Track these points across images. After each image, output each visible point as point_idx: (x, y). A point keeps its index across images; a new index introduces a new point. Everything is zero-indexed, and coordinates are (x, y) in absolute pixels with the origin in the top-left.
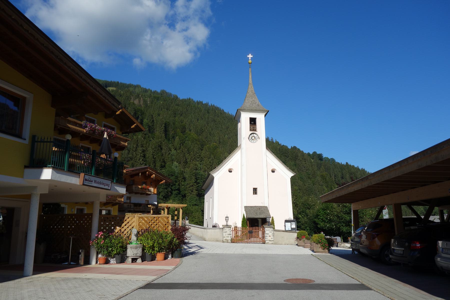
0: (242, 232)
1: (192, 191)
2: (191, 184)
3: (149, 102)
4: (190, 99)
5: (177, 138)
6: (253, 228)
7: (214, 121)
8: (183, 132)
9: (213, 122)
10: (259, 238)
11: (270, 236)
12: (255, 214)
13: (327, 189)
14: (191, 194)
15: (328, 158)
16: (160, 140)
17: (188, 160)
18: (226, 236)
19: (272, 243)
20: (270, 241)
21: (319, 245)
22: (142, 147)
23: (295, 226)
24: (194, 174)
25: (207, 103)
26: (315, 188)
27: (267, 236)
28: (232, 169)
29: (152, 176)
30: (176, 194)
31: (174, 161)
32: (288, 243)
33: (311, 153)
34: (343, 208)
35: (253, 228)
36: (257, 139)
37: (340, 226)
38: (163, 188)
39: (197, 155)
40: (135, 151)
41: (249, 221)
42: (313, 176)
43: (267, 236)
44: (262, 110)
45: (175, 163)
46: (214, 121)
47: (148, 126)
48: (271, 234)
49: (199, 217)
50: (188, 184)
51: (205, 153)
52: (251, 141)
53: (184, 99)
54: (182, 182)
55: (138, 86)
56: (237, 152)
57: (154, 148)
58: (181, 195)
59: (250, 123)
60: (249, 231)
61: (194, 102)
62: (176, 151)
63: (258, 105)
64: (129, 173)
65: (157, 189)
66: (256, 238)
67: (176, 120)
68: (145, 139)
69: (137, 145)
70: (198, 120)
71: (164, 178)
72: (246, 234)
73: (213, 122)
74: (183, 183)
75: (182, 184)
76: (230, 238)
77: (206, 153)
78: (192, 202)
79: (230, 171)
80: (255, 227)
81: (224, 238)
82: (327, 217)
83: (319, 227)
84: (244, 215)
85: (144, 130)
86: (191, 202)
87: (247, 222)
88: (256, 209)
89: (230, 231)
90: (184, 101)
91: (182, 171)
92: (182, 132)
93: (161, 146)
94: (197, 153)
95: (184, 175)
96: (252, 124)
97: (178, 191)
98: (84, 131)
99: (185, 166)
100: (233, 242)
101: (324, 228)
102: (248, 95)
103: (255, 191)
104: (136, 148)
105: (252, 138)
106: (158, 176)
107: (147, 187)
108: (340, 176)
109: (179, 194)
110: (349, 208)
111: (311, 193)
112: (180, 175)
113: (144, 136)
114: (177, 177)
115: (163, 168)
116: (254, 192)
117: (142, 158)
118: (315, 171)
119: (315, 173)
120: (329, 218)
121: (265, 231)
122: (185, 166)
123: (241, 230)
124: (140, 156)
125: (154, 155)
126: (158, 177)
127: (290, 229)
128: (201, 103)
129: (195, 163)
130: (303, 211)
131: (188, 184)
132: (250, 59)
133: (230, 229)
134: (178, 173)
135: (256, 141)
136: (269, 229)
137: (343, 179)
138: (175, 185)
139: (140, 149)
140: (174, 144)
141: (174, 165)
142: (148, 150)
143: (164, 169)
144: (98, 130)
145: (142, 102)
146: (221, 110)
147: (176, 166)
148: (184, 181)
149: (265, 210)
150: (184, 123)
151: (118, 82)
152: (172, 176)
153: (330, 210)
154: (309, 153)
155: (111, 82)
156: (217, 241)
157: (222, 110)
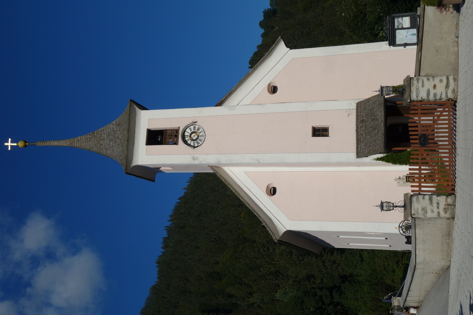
0: (422, 163)
1: (334, 262)
6: (411, 133)
7: (199, 216)
10: (436, 126)
11: (435, 87)
12: (376, 131)
14: (340, 264)
17: (273, 269)
18: (436, 210)
19: (455, 80)
20: (447, 86)
23: (404, 18)
24: (301, 258)
25: (166, 228)
27: (435, 95)
30: (341, 295)
33: (262, 31)
35: (411, 133)
36: (197, 127)
39: (263, 252)
43: (435, 95)
44: (129, 116)
45: (278, 295)
48: (429, 85)
49: (386, 259)
51: (258, 235)
53: (158, 273)
58: (342, 284)
59: (161, 143)
60: (420, 143)
61: (164, 253)
62: (254, 293)
63: (118, 125)
74: (318, 281)
75: (320, 282)
76: (442, 200)
77: (260, 233)
80: (410, 129)
81: (442, 214)
84: (378, 159)
86: (355, 266)
88: (363, 128)
91: (293, 281)
96: (162, 140)
97: (335, 290)
99: (285, 275)
100: (454, 190)
102: (95, 149)
105: (192, 140)
116: (323, 136)
121: (419, 99)
123: (418, 167)
127: (415, 31)
132: (15, 144)
134: (297, 290)
135: (201, 130)
136: (413, 89)
138: (321, 297)
141: (281, 299)
146: (181, 202)
147: (285, 293)
157: (179, 201)
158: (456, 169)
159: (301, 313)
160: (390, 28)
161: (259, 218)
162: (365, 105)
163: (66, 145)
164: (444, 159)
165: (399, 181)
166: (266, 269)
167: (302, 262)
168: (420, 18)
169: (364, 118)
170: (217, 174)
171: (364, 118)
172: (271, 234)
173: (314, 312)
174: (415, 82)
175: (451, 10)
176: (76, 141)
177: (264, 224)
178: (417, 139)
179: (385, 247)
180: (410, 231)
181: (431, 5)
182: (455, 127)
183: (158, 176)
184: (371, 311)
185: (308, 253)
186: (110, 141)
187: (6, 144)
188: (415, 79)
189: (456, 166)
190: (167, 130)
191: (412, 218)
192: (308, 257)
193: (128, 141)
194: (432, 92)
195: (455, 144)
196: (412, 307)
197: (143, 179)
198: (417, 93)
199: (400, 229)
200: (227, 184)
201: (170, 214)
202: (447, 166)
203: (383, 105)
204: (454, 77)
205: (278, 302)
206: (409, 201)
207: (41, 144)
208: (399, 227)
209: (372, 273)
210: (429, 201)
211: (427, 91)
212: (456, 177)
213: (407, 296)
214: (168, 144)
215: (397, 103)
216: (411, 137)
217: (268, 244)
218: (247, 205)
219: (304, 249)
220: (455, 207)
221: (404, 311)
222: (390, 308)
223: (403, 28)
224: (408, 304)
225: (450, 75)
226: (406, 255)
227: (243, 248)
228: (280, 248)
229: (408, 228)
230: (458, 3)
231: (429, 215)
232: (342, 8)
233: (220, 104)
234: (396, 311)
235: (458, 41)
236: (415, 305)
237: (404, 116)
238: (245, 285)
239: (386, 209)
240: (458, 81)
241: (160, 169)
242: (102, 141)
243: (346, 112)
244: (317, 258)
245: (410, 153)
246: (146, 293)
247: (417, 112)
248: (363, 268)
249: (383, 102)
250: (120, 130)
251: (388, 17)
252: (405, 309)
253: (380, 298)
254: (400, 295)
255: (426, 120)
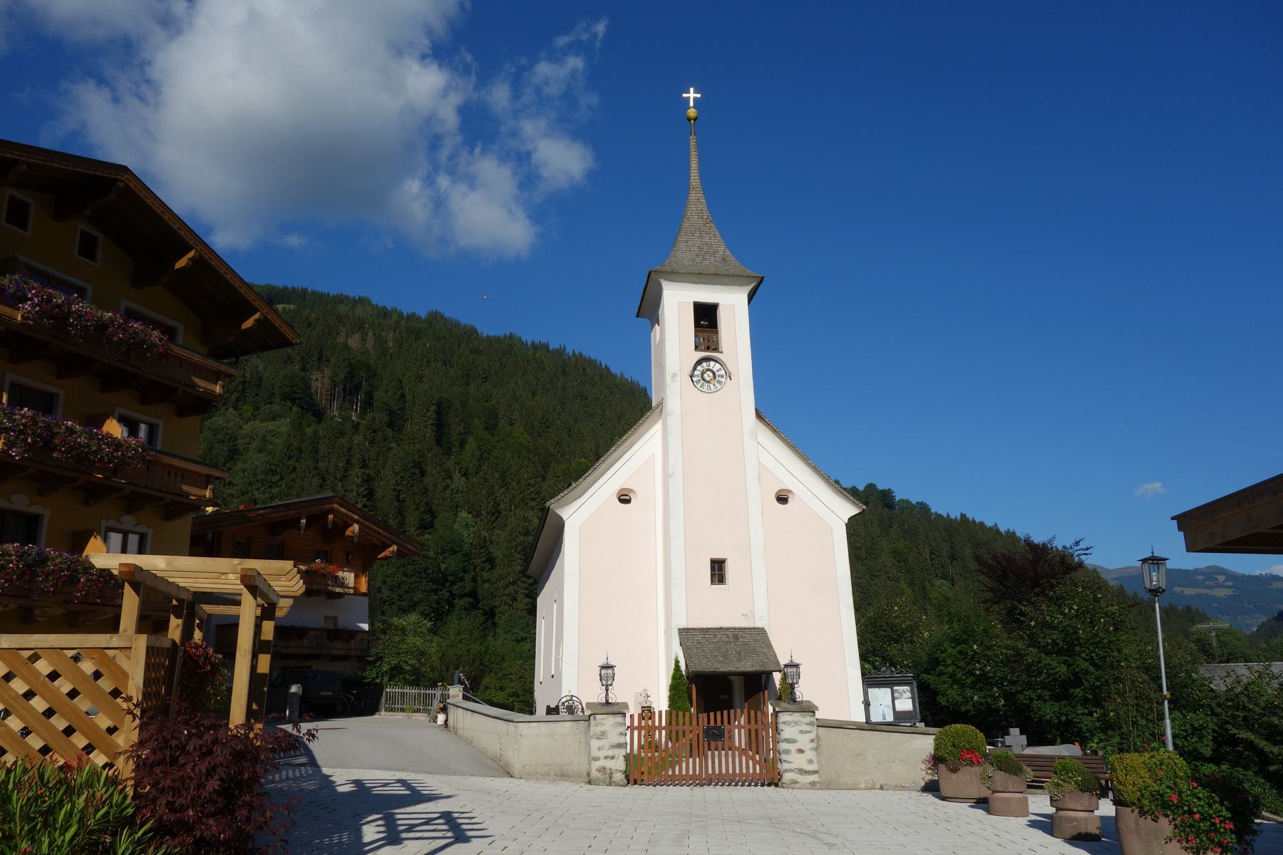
1: (514, 599)
2: (511, 576)
3: (391, 344)
4: (511, 336)
5: (471, 443)
7: (582, 396)
8: (491, 427)
9: (578, 401)
11: (801, 751)
13: (911, 591)
15: (911, 503)
16: (418, 446)
17: (502, 506)
18: (601, 754)
19: (813, 784)
20: (802, 772)
21: (1164, 822)
22: (365, 466)
23: (910, 700)
24: (519, 548)
25: (562, 347)
26: (876, 589)
27: (787, 752)
28: (631, 491)
29: (351, 529)
30: (465, 609)
31: (459, 509)
32: (882, 782)
33: (861, 488)
34: (1043, 632)
36: (723, 380)
37: (1031, 700)
38: (425, 590)
40: (341, 480)
41: (696, 686)
42: (868, 552)
43: (787, 752)
44: (738, 276)
45: (464, 514)
46: (582, 396)
47: (389, 410)
48: (804, 741)
49: (521, 677)
50: (501, 578)
52: (699, 386)
54: (483, 571)
55: (363, 301)
56: (648, 430)
57: (399, 472)
58: (481, 611)
59: (697, 325)
60: (709, 729)
62: (468, 479)
64: (260, 517)
65: (369, 576)
66: (723, 752)
67: (469, 393)
68: (374, 444)
69: (348, 462)
70: (534, 394)
71: (394, 538)
72: (695, 745)
73: (578, 401)
74: (486, 575)
76: (620, 764)
78: (515, 631)
79: (624, 499)
80: (725, 712)
81: (596, 765)
82: (970, 667)
83: (944, 704)
84: (677, 662)
85: (294, 342)
86: (509, 631)
87: (689, 690)
88: (725, 639)
89: (622, 729)
90: (492, 341)
91: (485, 537)
92: (487, 429)
93: (423, 465)
94: (529, 484)
95: (491, 550)
96: (702, 326)
97: (472, 600)
98: (12, 319)
99: (494, 525)
100: (635, 783)
101: (963, 709)
102: (686, 224)
103: (718, 570)
104: (346, 470)
105: (703, 373)
106: (370, 528)
107: (331, 568)
108: (945, 553)
109: (475, 607)
110: (1063, 631)
111: (864, 603)
112: (476, 552)
113: (372, 435)
114: (468, 557)
115: (427, 531)
116: (713, 576)
117: (361, 502)
118: (873, 539)
119: (874, 544)
120: (978, 673)
121: (781, 727)
122: (492, 525)
123: (664, 724)
124: (358, 492)
125: (399, 491)
126: (371, 532)
127: (890, 718)
128: (545, 347)
129: (522, 513)
130: (874, 650)
131: (501, 578)
132: (692, 104)
133: (619, 719)
134: (471, 543)
135: (719, 386)
136: (796, 717)
137: (955, 561)
138: (462, 580)
139: (356, 474)
140: (460, 457)
142: (381, 478)
143: (430, 534)
144: (80, 316)
145: (372, 343)
148: (489, 570)
149: (758, 640)
150: (493, 402)
151: (305, 290)
152: (454, 552)
153: (982, 644)
154: (855, 487)
155: (286, 288)
156: (563, 776)
157: (603, 367)
158: (669, 786)
159: (437, 549)
160: (895, 679)
161: (583, 477)
162: (761, 640)
163: (692, 181)
164: (677, 769)
165: (643, 695)
166: (503, 496)
167: (513, 550)
168: (912, 726)
169: (741, 640)
170: (651, 411)
171: (741, 640)
172: (559, 497)
173: (440, 570)
174: (808, 719)
175: (929, 778)
176: (698, 195)
177: (574, 485)
178: (715, 723)
179: (540, 674)
180: (565, 712)
181: (936, 744)
182: (736, 785)
183: (646, 321)
184: (441, 654)
185: (528, 560)
186: (699, 247)
187: (692, 90)
188: (813, 719)
189: (674, 786)
190: (717, 328)
191: (590, 716)
192: (521, 559)
193: (700, 273)
194: (793, 747)
195: (709, 785)
196: (447, 716)
197: (640, 299)
198: (790, 722)
199: (568, 698)
200: (635, 427)
201: (584, 353)
202: (667, 772)
203: (762, 669)
204: (818, 782)
205: (454, 515)
206: (616, 711)
207: (693, 143)
208: (572, 696)
209: (498, 656)
210: (617, 742)
211: (794, 739)
212: (655, 786)
213: (464, 709)
214: (696, 336)
215: (766, 691)
216: (712, 714)
217: (540, 500)
218: (602, 459)
219: (535, 549)
220: (607, 785)
221: (442, 705)
222: (445, 683)
223: (893, 699)
224: (451, 710)
225: (820, 776)
226: (527, 706)
227: (533, 463)
228: (534, 517)
229: (571, 710)
230: (941, 790)
231: (595, 744)
232: (906, 606)
233: (759, 415)
234: (440, 692)
235: (875, 789)
236: (450, 722)
237: (746, 702)
238: (479, 465)
239: (603, 674)
240: (811, 789)
241: (657, 325)
242: (698, 235)
243: (750, 612)
244: (520, 572)
245: (688, 710)
246: (465, 319)
247: (753, 722)
248: (506, 642)
249: (768, 669)
250: (716, 262)
251: (912, 675)
252: (445, 706)
253: (461, 668)
254: (465, 698)
255: (739, 737)
